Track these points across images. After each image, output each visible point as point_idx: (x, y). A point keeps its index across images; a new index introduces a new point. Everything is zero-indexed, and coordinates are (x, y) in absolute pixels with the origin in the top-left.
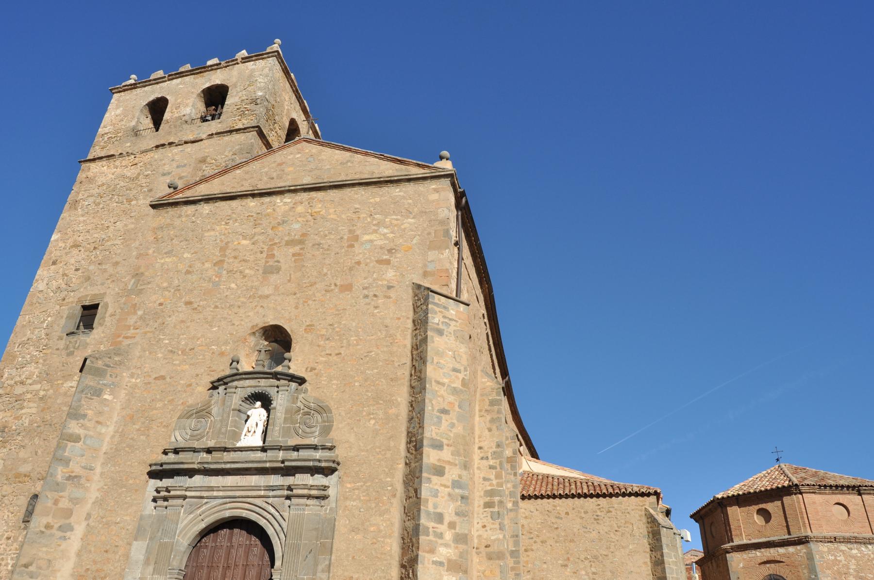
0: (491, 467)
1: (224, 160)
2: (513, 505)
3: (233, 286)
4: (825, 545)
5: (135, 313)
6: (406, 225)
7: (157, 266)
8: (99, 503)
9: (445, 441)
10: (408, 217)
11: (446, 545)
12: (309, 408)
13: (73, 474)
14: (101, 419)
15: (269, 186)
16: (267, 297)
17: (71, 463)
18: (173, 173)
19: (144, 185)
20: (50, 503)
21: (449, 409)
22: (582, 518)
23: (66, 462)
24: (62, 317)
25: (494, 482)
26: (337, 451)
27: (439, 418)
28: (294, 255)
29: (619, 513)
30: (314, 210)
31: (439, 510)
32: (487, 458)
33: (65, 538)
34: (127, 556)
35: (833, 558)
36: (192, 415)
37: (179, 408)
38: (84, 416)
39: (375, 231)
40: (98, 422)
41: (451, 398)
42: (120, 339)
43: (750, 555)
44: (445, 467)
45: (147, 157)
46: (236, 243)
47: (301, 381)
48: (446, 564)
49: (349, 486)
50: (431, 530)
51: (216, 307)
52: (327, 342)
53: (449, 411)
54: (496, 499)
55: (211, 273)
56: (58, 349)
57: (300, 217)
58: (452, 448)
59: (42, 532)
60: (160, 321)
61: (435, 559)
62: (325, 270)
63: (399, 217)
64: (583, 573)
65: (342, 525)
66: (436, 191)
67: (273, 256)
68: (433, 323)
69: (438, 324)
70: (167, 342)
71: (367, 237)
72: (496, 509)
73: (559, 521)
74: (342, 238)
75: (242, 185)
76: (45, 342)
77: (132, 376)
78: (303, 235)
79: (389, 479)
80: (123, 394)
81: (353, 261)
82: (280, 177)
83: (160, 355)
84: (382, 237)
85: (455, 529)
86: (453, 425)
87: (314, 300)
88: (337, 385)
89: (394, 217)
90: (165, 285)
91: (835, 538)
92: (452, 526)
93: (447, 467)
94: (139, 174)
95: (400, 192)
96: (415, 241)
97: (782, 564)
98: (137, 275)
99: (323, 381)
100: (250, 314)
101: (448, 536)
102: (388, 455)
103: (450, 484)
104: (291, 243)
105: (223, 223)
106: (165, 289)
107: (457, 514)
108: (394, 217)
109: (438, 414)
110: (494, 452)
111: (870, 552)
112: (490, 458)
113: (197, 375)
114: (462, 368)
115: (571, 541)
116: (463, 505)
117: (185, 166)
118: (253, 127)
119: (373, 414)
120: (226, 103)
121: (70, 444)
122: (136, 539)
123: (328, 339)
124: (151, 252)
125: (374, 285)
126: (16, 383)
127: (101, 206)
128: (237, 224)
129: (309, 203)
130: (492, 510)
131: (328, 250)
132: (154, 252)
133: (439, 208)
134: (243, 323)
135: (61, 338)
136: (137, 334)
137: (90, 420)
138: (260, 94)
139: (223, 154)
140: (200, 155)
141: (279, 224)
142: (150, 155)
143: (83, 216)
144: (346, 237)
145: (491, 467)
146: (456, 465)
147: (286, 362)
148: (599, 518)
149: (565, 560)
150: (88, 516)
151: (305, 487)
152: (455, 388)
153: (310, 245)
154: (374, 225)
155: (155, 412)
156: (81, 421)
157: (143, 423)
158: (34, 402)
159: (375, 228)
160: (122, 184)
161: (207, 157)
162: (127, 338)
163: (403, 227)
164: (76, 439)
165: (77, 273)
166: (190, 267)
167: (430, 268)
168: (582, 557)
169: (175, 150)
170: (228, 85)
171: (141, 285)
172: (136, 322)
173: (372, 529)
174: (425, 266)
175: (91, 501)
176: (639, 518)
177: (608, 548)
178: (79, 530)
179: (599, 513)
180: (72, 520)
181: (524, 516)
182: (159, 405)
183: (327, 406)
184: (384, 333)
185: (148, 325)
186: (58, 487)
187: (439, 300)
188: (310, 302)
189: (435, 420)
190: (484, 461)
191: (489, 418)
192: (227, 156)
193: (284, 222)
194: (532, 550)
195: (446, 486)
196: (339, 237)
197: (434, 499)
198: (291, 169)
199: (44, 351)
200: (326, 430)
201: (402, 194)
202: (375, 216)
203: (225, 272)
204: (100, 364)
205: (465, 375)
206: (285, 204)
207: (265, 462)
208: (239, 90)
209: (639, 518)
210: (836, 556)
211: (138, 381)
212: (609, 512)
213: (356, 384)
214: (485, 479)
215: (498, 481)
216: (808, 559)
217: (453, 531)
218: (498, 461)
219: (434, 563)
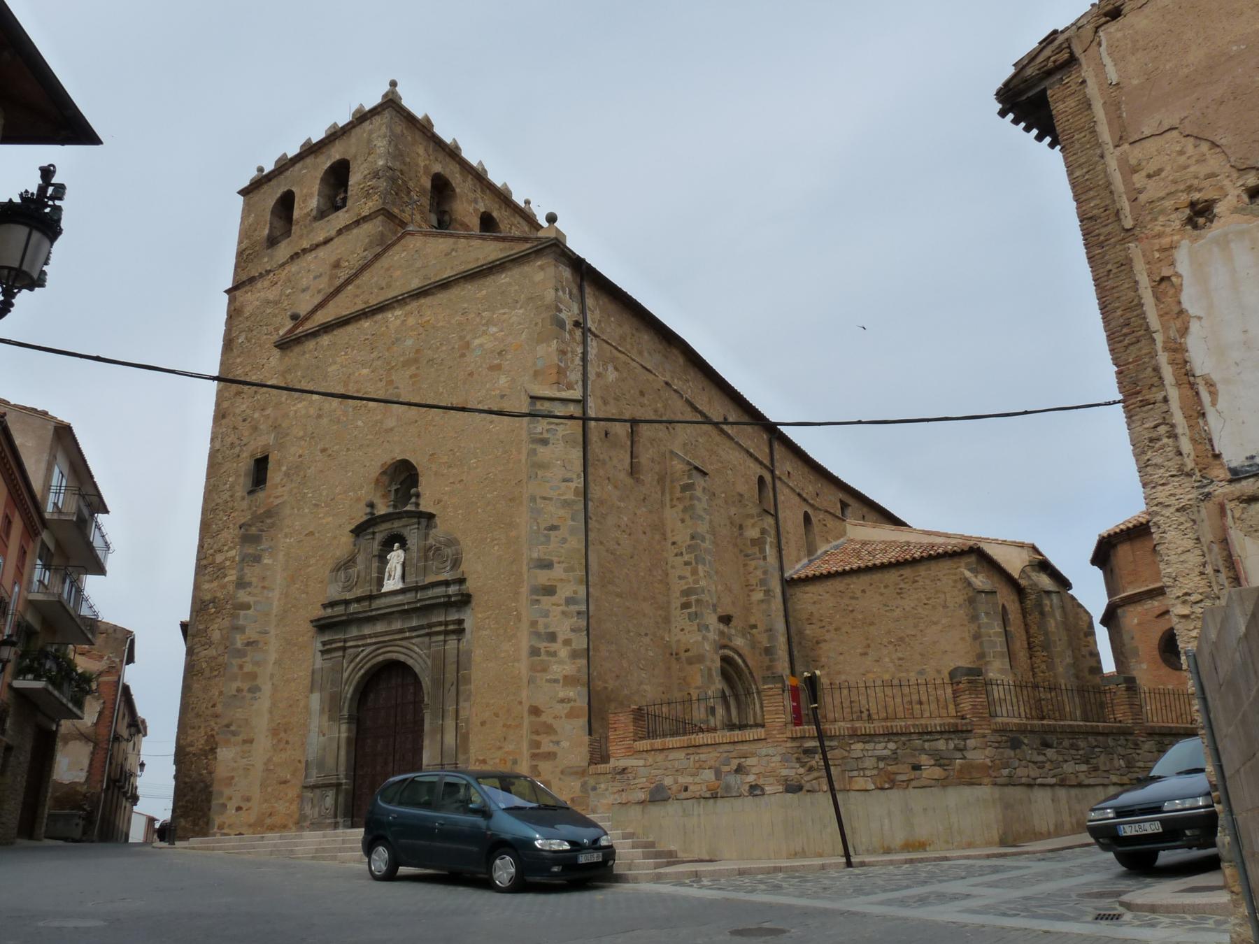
0: (686, 563)
1: (356, 259)
2: (765, 595)
3: (360, 423)
5: (280, 470)
6: (514, 319)
7: (291, 414)
8: (278, 662)
9: (555, 559)
10: (515, 308)
11: (561, 662)
12: (440, 542)
13: (251, 640)
14: (266, 584)
15: (381, 299)
16: (391, 429)
17: (247, 630)
18: (312, 287)
19: (287, 307)
20: (235, 670)
21: (559, 524)
22: (882, 594)
23: (241, 629)
24: (240, 475)
25: (691, 580)
26: (468, 583)
27: (548, 537)
28: (411, 377)
29: (928, 582)
30: (425, 319)
31: (551, 630)
32: (681, 554)
33: (256, 699)
34: (307, 707)
36: (341, 568)
37: (329, 561)
38: (249, 584)
39: (484, 333)
40: (264, 587)
41: (561, 512)
42: (271, 499)
43: (1145, 607)
44: (556, 586)
45: (283, 274)
46: (357, 374)
47: (431, 516)
48: (561, 681)
49: (480, 616)
50: (542, 651)
51: (348, 450)
52: (450, 469)
53: (559, 526)
54: (694, 598)
55: (339, 413)
56: (243, 511)
57: (412, 331)
58: (564, 565)
59: (235, 696)
60: (302, 474)
61: (548, 677)
62: (441, 390)
63: (506, 310)
64: (887, 660)
65: (478, 655)
66: (541, 268)
67: (392, 382)
68: (535, 434)
69: (541, 433)
70: (310, 495)
71: (477, 342)
72: (693, 610)
73: (853, 602)
74: (453, 348)
75: (355, 304)
76: (230, 504)
77: (286, 536)
78: (418, 351)
79: (513, 604)
80: (281, 556)
81: (466, 373)
82: (389, 286)
83: (307, 511)
84: (492, 338)
85: (571, 646)
86: (564, 540)
87: (434, 426)
88: (462, 514)
89: (502, 311)
90: (301, 434)
92: (567, 642)
93: (559, 585)
94: (281, 296)
95: (506, 277)
96: (524, 336)
100: (378, 452)
101: (563, 653)
102: (512, 580)
103: (563, 602)
104: (406, 364)
105: (343, 353)
106: (302, 438)
107: (572, 630)
108: (502, 311)
109: (546, 532)
110: (689, 546)
112: (684, 553)
113: (340, 526)
114: (575, 476)
115: (870, 625)
116: (580, 620)
117: (321, 275)
118: (378, 210)
119: (496, 539)
120: (350, 183)
121: (242, 613)
122: (312, 692)
123: (450, 467)
124: (283, 399)
125: (488, 397)
126: (215, 552)
127: (253, 341)
128: (355, 351)
129: (419, 312)
130: (689, 610)
131: (441, 364)
132: (287, 399)
133: (545, 290)
134: (373, 463)
135: (243, 498)
136: (283, 492)
137: (256, 587)
138: (381, 163)
139: (355, 253)
140: (333, 259)
141: (393, 343)
142: (287, 268)
143: (239, 356)
144: (457, 346)
145: (686, 563)
146: (570, 581)
147: (413, 500)
148: (903, 591)
149: (865, 647)
150: (272, 676)
151: (440, 624)
152: (565, 501)
153: (425, 362)
154: (483, 325)
155: (310, 568)
156: (249, 589)
157: (302, 582)
158: (233, 569)
159: (484, 328)
160: (268, 311)
161: (340, 259)
162: (277, 497)
163: (511, 321)
164: (246, 607)
165: (245, 424)
166: (320, 410)
167: (540, 365)
168: (885, 641)
169: (310, 257)
170: (348, 158)
171: (281, 438)
172: (282, 480)
173: (503, 655)
174: (535, 364)
175: (272, 662)
176: (953, 584)
177: (916, 626)
178: (267, 689)
179: (902, 585)
180: (259, 682)
181: (812, 601)
182: (312, 561)
183: (455, 539)
184: (501, 450)
185: (292, 480)
186: (240, 654)
187: (542, 405)
188: (431, 428)
189: (543, 539)
190: (679, 558)
191: (681, 507)
192: (358, 254)
193: (397, 340)
194: (825, 641)
195: (558, 605)
196: (450, 348)
197: (545, 620)
198: (398, 273)
199: (232, 515)
200: (456, 563)
201: (507, 279)
202: (483, 314)
203: (351, 410)
204: (253, 530)
205: (579, 483)
206: (397, 317)
207: (404, 604)
208: (360, 162)
209: (953, 584)
211: (292, 540)
212: (915, 582)
213: (479, 510)
214: (681, 578)
215: (694, 577)
217: (569, 648)
218: (693, 556)
219: (548, 681)
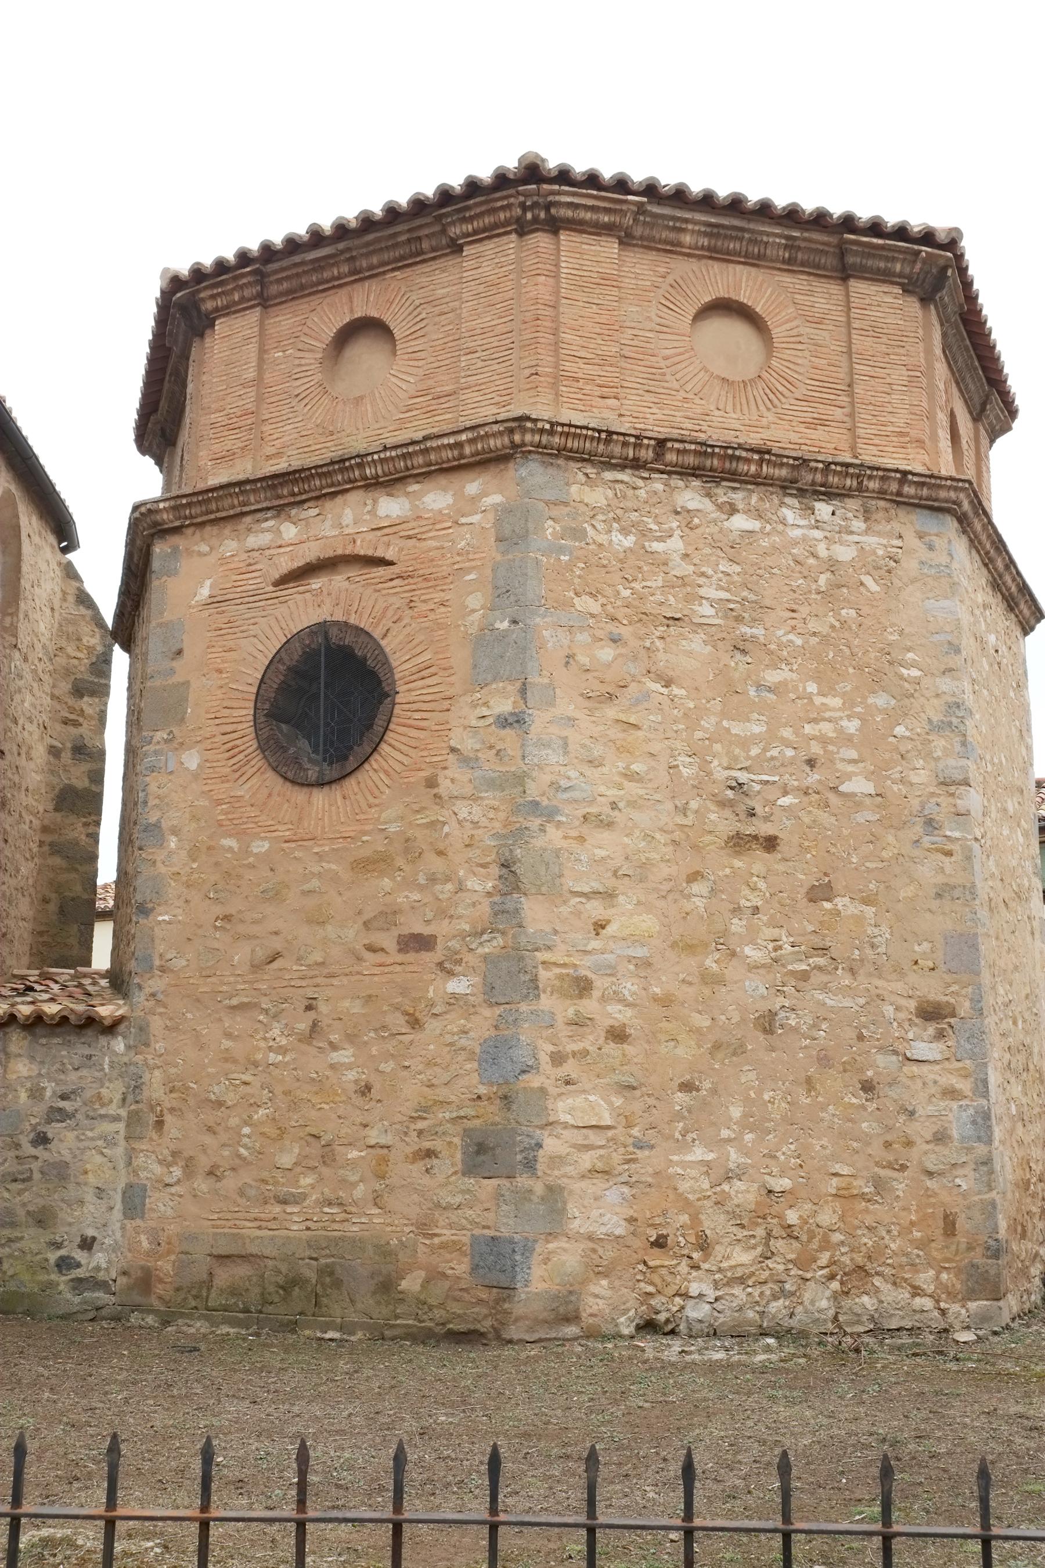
4: (609, 475)
35: (629, 541)
91: (661, 443)
97: (381, 572)
98: (939, 896)
99: (349, 1067)
111: (817, 534)
210: (644, 533)
216: (500, 540)
